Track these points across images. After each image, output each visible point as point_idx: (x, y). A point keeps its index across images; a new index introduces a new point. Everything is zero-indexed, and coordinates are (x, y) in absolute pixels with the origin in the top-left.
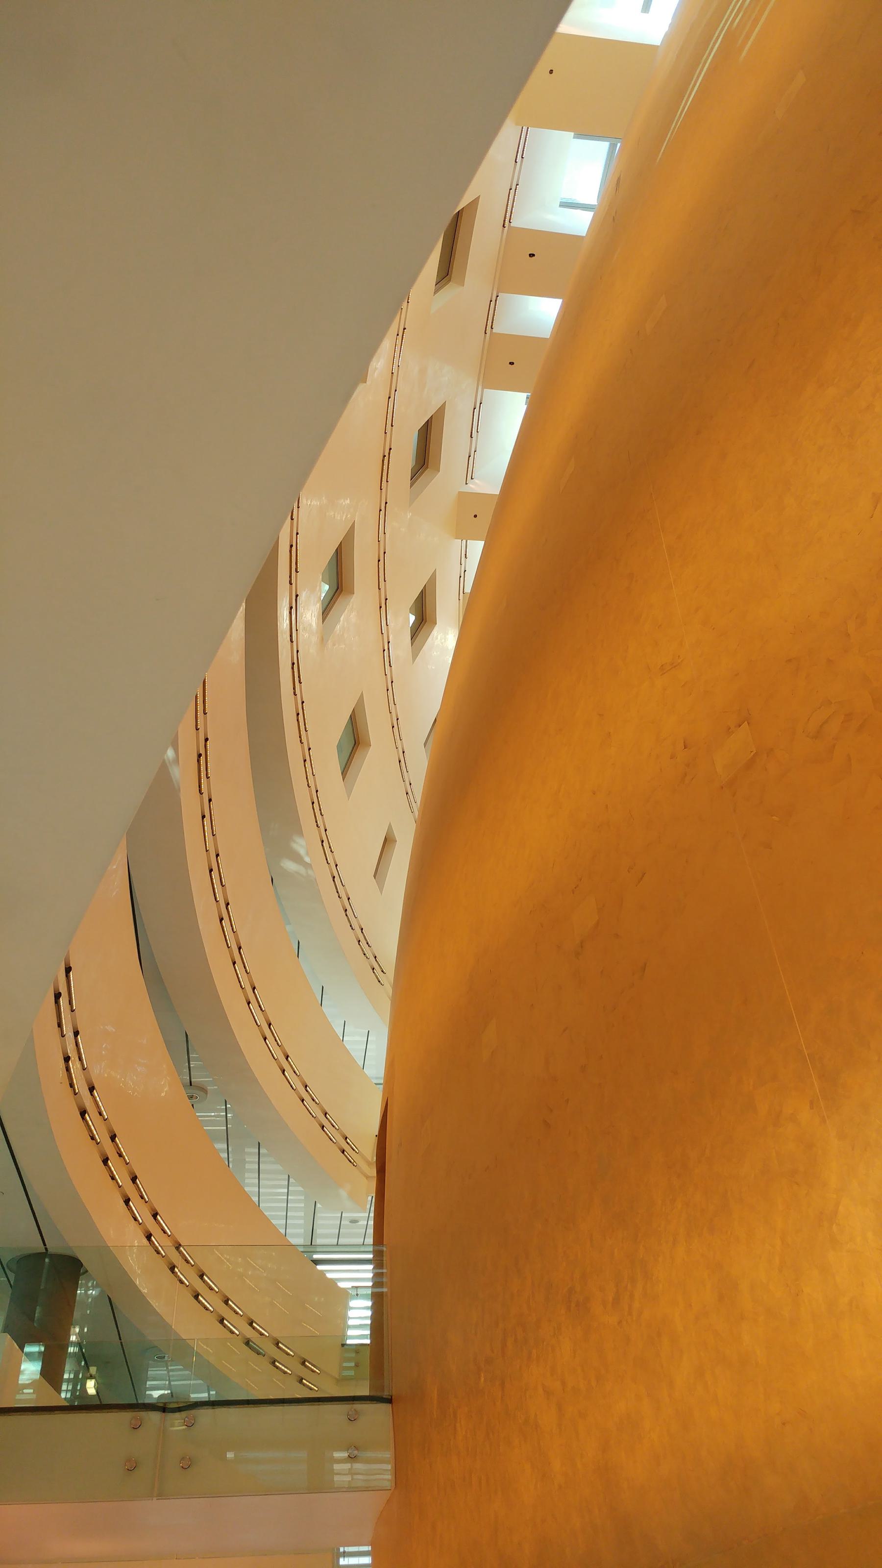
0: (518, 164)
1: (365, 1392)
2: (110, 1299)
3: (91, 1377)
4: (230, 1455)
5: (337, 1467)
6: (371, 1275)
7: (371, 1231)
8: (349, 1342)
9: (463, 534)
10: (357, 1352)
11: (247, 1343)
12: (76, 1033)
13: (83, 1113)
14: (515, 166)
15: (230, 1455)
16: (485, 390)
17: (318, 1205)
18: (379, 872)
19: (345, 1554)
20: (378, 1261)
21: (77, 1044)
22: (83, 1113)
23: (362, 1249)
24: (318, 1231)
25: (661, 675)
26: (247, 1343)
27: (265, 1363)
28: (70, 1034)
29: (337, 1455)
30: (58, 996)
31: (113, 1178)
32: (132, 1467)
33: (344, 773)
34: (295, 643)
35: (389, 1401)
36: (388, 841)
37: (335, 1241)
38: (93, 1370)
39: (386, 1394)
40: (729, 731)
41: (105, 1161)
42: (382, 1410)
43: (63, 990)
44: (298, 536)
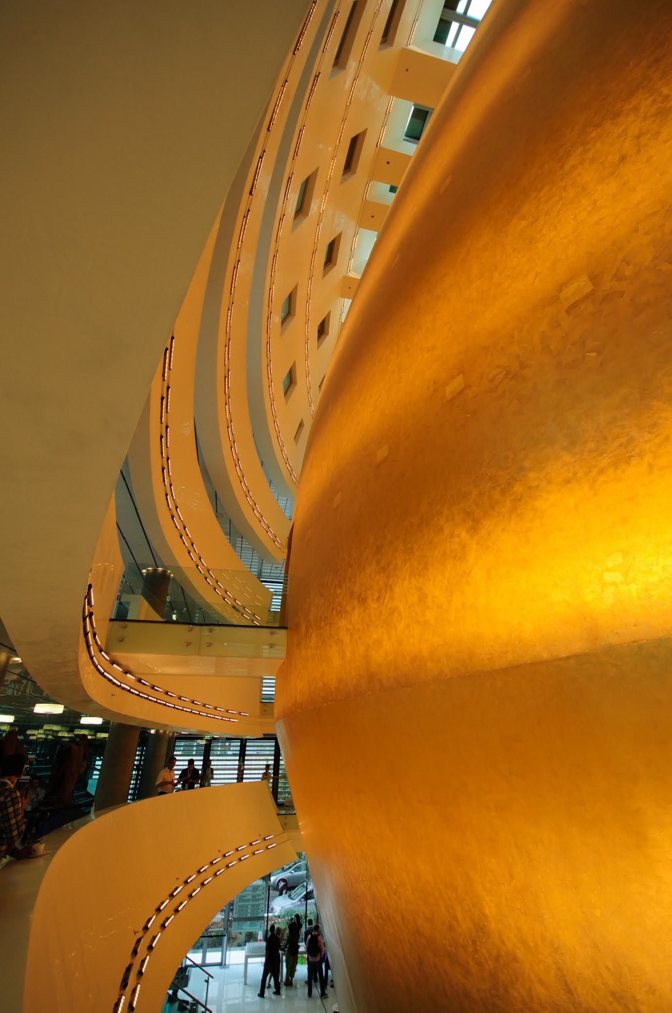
0: (387, 115)
1: (277, 625)
2: (182, 588)
3: (174, 614)
4: (225, 644)
5: (264, 651)
6: (282, 587)
7: (284, 569)
8: (271, 610)
9: (344, 295)
10: (275, 614)
11: (234, 607)
12: (171, 485)
13: (173, 517)
14: (386, 116)
15: (225, 644)
16: (360, 228)
17: (264, 561)
18: (296, 437)
19: (265, 679)
20: (285, 583)
21: (171, 490)
22: (173, 517)
23: (279, 578)
24: (263, 567)
25: (371, 578)
26: (234, 607)
27: (240, 614)
28: (165, 459)
29: (265, 647)
30: (163, 469)
31: (184, 543)
32: (188, 644)
33: (285, 394)
34: (273, 278)
35: (286, 628)
36: (301, 425)
37: (269, 571)
38: (175, 611)
39: (285, 626)
40: (454, 377)
41: (181, 537)
42: (283, 632)
43: (164, 435)
44: (287, 83)
